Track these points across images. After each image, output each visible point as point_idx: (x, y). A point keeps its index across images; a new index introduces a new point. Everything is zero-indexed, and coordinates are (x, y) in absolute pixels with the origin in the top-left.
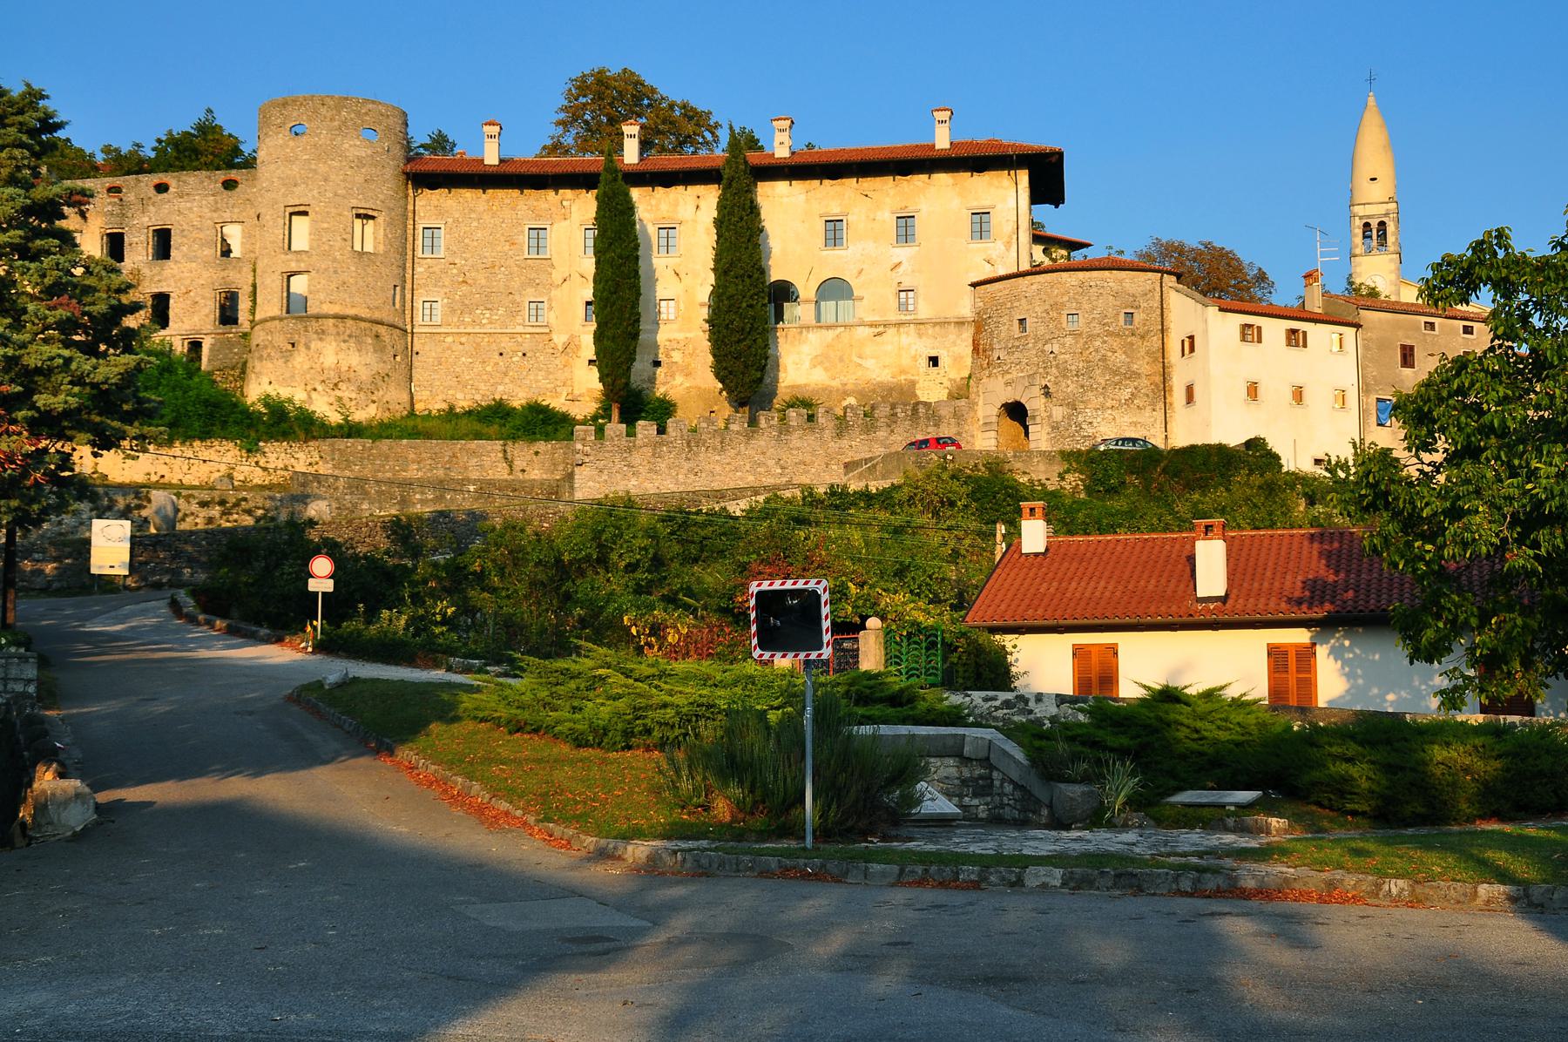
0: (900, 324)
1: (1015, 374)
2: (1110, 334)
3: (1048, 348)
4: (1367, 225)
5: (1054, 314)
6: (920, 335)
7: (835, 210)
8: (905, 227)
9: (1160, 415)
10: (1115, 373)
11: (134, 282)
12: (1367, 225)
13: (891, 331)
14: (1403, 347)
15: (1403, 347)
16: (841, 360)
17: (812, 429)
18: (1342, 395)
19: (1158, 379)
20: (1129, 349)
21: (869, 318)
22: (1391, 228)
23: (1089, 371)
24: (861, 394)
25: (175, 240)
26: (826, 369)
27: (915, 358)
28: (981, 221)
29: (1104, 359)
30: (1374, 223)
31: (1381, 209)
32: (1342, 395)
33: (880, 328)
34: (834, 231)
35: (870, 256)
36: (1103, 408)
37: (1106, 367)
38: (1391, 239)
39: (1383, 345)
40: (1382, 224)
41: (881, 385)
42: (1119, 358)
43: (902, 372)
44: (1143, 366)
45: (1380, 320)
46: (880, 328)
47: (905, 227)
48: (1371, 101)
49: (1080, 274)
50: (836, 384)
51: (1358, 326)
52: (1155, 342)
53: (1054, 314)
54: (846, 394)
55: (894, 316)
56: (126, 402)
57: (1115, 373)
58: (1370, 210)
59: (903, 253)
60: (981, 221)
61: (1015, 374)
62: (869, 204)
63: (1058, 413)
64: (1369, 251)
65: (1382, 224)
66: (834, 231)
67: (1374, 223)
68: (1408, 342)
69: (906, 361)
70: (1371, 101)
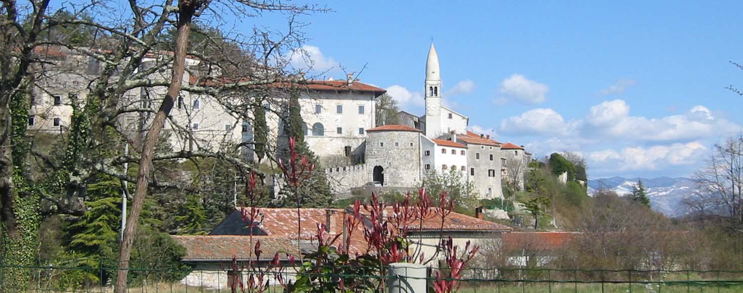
4: (431, 87)
6: (343, 142)
8: (340, 109)
11: (638, 180)
12: (431, 87)
13: (335, 139)
16: (320, 147)
20: (411, 153)
22: (438, 89)
25: (480, 155)
28: (361, 110)
30: (433, 87)
31: (435, 83)
34: (318, 109)
38: (438, 93)
40: (436, 88)
42: (409, 156)
56: (569, 178)
59: (339, 116)
62: (329, 104)
65: (436, 88)
66: (318, 109)
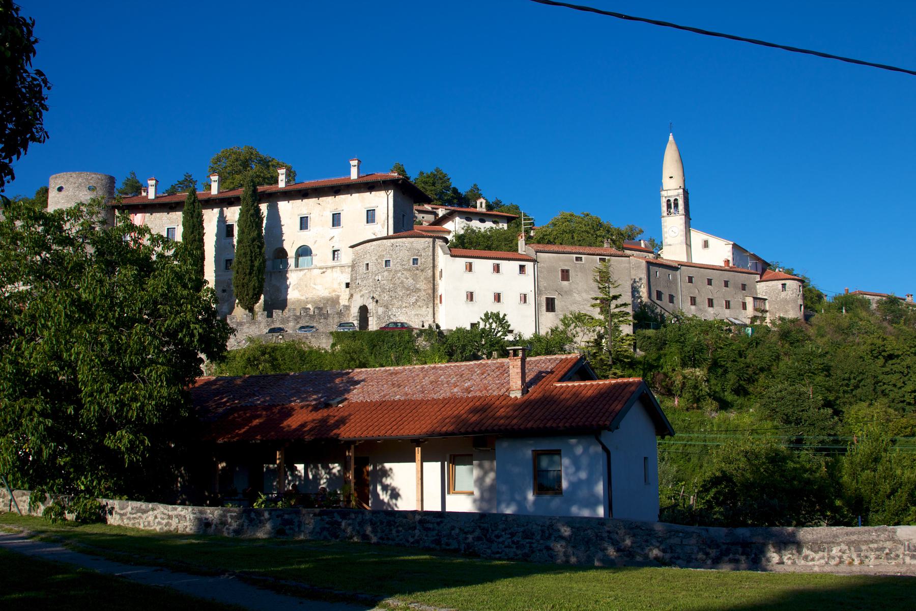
0: (333, 267)
1: (364, 291)
2: (405, 270)
3: (377, 278)
4: (669, 201)
5: (379, 261)
7: (304, 213)
8: (336, 220)
9: (431, 310)
10: (408, 289)
12: (669, 201)
13: (329, 271)
14: (563, 271)
15: (563, 271)
17: (255, 323)
18: (524, 298)
19: (430, 292)
20: (415, 278)
21: (319, 265)
23: (394, 289)
24: (313, 302)
26: (299, 291)
27: (339, 284)
28: (371, 216)
29: (402, 282)
30: (672, 200)
31: (676, 193)
32: (524, 298)
33: (324, 269)
34: (304, 223)
35: (320, 236)
36: (400, 307)
37: (403, 287)
39: (551, 270)
40: (676, 200)
41: (323, 298)
43: (334, 291)
44: (423, 285)
45: (549, 257)
46: (324, 269)
47: (336, 220)
48: (671, 138)
49: (392, 241)
50: (303, 298)
51: (535, 261)
52: (430, 273)
53: (379, 261)
54: (307, 303)
55: (331, 263)
57: (408, 289)
58: (670, 193)
60: (371, 216)
61: (364, 291)
63: (381, 310)
64: (669, 213)
65: (676, 200)
67: (672, 200)
68: (566, 268)
69: (336, 286)
70: (671, 138)
